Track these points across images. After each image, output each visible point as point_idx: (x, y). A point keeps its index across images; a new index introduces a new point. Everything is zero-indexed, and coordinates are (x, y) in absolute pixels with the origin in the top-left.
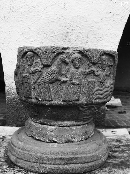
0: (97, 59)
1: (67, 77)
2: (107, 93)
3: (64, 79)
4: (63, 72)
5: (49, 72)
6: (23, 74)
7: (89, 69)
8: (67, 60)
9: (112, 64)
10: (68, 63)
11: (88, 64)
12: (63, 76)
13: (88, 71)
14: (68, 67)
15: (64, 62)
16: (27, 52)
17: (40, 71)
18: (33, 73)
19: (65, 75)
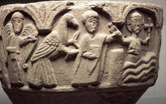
1: (77, 48)
2: (146, 71)
3: (71, 50)
4: (70, 41)
8: (76, 21)
11: (110, 27)
13: (110, 36)
15: (71, 26)
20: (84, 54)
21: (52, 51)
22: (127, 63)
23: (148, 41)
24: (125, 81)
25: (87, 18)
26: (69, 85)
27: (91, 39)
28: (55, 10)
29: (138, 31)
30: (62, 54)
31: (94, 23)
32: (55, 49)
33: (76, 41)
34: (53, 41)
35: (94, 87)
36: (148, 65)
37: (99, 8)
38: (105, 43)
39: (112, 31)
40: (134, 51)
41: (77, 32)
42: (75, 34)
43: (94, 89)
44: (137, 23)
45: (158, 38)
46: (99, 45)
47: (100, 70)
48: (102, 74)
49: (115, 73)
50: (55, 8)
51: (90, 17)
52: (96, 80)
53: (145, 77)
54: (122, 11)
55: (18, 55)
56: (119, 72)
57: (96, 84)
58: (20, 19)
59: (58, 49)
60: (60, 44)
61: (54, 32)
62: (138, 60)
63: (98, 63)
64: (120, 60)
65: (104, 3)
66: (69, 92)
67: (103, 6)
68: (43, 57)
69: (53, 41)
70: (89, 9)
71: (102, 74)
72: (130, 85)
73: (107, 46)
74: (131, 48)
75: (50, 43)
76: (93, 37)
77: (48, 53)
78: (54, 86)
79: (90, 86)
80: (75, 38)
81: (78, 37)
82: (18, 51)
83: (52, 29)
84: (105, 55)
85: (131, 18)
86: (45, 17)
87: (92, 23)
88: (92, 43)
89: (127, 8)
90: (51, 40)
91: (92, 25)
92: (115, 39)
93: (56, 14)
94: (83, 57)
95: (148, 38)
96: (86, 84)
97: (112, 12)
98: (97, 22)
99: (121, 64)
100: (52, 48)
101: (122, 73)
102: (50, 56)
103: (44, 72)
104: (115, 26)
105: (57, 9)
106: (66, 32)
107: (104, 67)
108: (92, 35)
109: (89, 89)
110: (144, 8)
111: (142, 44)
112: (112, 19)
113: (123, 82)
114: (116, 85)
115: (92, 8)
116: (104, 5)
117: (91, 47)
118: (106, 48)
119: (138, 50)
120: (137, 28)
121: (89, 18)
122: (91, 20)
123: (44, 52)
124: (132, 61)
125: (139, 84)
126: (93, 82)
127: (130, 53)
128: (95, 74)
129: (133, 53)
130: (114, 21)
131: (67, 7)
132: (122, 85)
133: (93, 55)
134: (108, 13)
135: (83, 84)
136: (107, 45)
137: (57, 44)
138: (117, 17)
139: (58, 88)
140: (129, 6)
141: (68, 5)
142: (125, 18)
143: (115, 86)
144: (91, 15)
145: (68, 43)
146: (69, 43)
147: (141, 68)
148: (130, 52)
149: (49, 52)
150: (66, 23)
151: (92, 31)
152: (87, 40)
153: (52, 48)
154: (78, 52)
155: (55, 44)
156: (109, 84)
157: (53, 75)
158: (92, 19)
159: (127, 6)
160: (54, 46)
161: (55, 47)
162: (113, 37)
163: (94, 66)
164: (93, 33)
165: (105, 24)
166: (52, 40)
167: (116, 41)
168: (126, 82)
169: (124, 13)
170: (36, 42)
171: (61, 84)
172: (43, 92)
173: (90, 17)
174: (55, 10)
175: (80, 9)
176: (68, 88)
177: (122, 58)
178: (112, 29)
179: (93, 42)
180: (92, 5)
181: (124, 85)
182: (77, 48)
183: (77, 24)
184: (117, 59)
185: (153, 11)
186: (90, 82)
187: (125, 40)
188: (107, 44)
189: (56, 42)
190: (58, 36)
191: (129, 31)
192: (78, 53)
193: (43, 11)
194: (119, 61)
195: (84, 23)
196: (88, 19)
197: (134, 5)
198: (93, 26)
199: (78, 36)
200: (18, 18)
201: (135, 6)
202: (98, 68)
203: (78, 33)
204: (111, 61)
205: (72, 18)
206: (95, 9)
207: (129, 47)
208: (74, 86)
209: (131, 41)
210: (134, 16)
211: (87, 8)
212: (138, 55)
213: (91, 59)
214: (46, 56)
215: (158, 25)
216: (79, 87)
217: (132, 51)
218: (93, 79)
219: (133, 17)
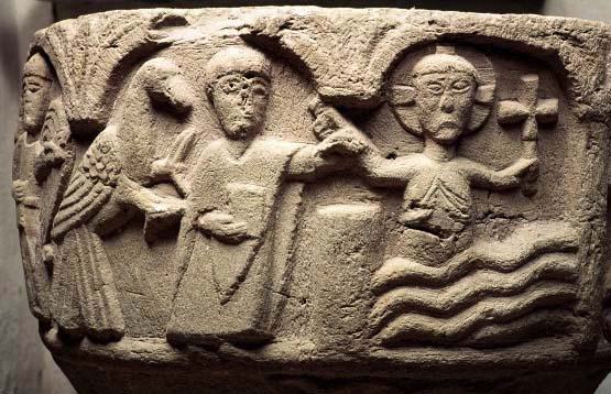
1: (182, 195)
2: (503, 306)
3: (157, 202)
4: (159, 165)
7: (320, 139)
8: (180, 90)
11: (312, 113)
13: (308, 152)
15: (168, 110)
20: (202, 221)
21: (97, 200)
22: (395, 265)
23: (523, 174)
24: (384, 340)
25: (219, 77)
26: (159, 336)
27: (233, 162)
28: (113, 45)
29: (448, 134)
30: (130, 217)
31: (244, 97)
32: (109, 196)
33: (182, 165)
34: (100, 166)
35: (246, 354)
36: (512, 280)
37: (266, 37)
38: (287, 179)
39: (318, 129)
40: (430, 217)
41: (187, 132)
42: (178, 137)
43: (248, 359)
44: (443, 97)
45: (590, 163)
46: (265, 188)
47: (267, 287)
48: (282, 305)
49: (333, 303)
50: (115, 37)
51: (229, 73)
52: (248, 327)
53: (493, 330)
54: (365, 47)
55: (30, 210)
56: (353, 301)
57: (256, 340)
58: (36, 80)
59: (116, 194)
60: (123, 176)
61: (110, 133)
62: (450, 256)
63: (259, 260)
64: (357, 250)
65: (286, 17)
66: (161, 366)
67: (282, 28)
68: (77, 225)
69: (100, 166)
70: (234, 40)
71: (282, 305)
72: (410, 355)
73: (301, 190)
74: (414, 205)
75: (93, 173)
76: (242, 153)
77: (88, 209)
78: (115, 336)
79: (226, 347)
80: (177, 155)
81: (187, 152)
82: (30, 198)
83: (107, 120)
84: (292, 227)
85: (415, 76)
86: (83, 74)
87: (237, 99)
88: (238, 178)
89: (391, 34)
90: (94, 160)
91: (238, 110)
92: (331, 162)
93: (115, 62)
94: (197, 228)
95: (522, 163)
96: (208, 337)
97: (320, 51)
98: (259, 92)
99: (363, 266)
100: (99, 193)
101: (371, 306)
102: (96, 221)
103: (82, 280)
104: (331, 111)
105: (119, 43)
106: (143, 130)
107: (288, 276)
108: (237, 144)
109: (226, 360)
110: (489, 32)
111: (478, 185)
112: (318, 80)
113: (373, 340)
114: (341, 351)
115: (242, 36)
116: (286, 25)
117: (228, 194)
118: (299, 200)
119: (447, 211)
120: (445, 118)
121: (223, 78)
122: (232, 86)
123: (79, 206)
124: (418, 257)
125: (461, 357)
126: (238, 334)
127: (410, 225)
128: (247, 300)
129: (422, 225)
130: (328, 91)
131: (154, 32)
132: (374, 354)
133: (237, 225)
134: (299, 57)
135: (198, 336)
136: (299, 187)
137: (112, 176)
138: (338, 73)
139: (127, 346)
140: (406, 26)
141: (157, 24)
142: (378, 76)
143: (337, 357)
144: (229, 66)
145: (151, 174)
146: (157, 175)
147: (469, 291)
148: (408, 219)
149: (91, 207)
150: (145, 96)
151: (233, 128)
152: (213, 166)
153: (99, 193)
154: (182, 210)
155: (108, 178)
156: (312, 346)
157: (111, 294)
158: (235, 80)
159: (393, 27)
160: (105, 181)
161: (107, 189)
162: (324, 154)
163: (238, 269)
164: (243, 136)
165: (290, 100)
166: (99, 161)
167: (340, 170)
168: (389, 344)
169: (375, 57)
170: (65, 167)
171: (137, 330)
172: (85, 356)
173: (229, 73)
174: (113, 45)
175: (203, 42)
176: (154, 347)
177: (375, 242)
178: (319, 124)
179: (239, 174)
180: (245, 26)
181: (383, 353)
182: (182, 195)
183: (180, 100)
184: (338, 247)
185: (547, 46)
186: (226, 330)
187: (381, 167)
188: (300, 181)
189: (109, 167)
190: (116, 144)
191: (408, 131)
192: (179, 216)
193: (82, 49)
194: (348, 254)
195: (211, 99)
196: (221, 81)
197: (431, 23)
198: (238, 108)
199: (190, 146)
200: (31, 75)
201: (434, 27)
202: (254, 279)
203: (191, 134)
204: (314, 251)
205: (165, 78)
206: (254, 40)
207: (406, 197)
208: (175, 340)
209: (412, 175)
210: (427, 70)
211: (225, 37)
212: (448, 233)
213: (231, 241)
214: (87, 220)
215: (584, 107)
216: (190, 347)
217: (416, 217)
218: (238, 318)
219: (422, 71)
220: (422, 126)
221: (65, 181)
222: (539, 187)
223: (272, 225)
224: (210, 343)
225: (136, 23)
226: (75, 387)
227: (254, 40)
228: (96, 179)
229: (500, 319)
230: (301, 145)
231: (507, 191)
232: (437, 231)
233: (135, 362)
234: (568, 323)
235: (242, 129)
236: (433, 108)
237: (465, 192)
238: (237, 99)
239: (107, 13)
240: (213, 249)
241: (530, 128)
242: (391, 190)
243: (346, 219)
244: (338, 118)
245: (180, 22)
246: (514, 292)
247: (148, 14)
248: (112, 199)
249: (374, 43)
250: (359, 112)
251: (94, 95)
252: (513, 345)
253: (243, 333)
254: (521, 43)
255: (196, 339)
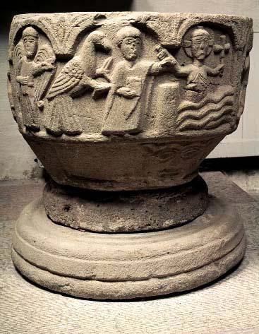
0: (179, 37)
1: (109, 81)
2: (215, 115)
3: (100, 85)
4: (99, 71)
5: (67, 70)
6: (97, 70)
7: (161, 60)
8: (106, 43)
9: (228, 45)
10: (251, 20)
11: (157, 51)
12: (100, 79)
13: (157, 65)
14: (109, 59)
15: (100, 50)
16: (24, 27)
17: (50, 70)
18: (37, 74)
19: (102, 76)
20: (118, 91)
30: (87, 90)
31: (134, 45)
32: (78, 83)
34: (74, 71)
36: (218, 106)
39: (160, 56)
43: (134, 138)
46: (140, 78)
53: (214, 123)
59: (81, 82)
61: (77, 58)
63: (140, 104)
69: (74, 71)
72: (188, 133)
74: (191, 82)
78: (78, 133)
79: (127, 135)
81: (110, 66)
87: (131, 46)
89: (186, 22)
91: (131, 49)
93: (79, 32)
94: (116, 94)
95: (220, 66)
98: (138, 44)
101: (177, 118)
102: (71, 92)
108: (130, 63)
111: (209, 74)
116: (149, 19)
120: (202, 52)
123: (63, 86)
124: (192, 100)
127: (190, 89)
128: (135, 118)
129: (193, 89)
130: (164, 43)
135: (116, 132)
136: (153, 78)
137: (80, 75)
139: (84, 137)
141: (96, 18)
146: (98, 75)
160: (76, 77)
162: (163, 66)
163: (132, 108)
164: (132, 60)
165: (150, 47)
167: (168, 71)
168: (182, 130)
169: (180, 30)
176: (97, 136)
177: (176, 96)
181: (180, 133)
182: (109, 81)
184: (167, 98)
187: (182, 70)
189: (78, 72)
191: (188, 56)
192: (109, 88)
196: (125, 40)
202: (138, 109)
206: (136, 24)
209: (190, 72)
213: (129, 98)
218: (132, 125)
220: (193, 54)
221: (52, 78)
222: (224, 74)
223: (144, 91)
224: (120, 135)
225: (88, 17)
226: (31, 146)
227: (136, 24)
228: (72, 76)
229: (215, 119)
230: (153, 62)
231: (215, 76)
232: (198, 91)
233: (87, 142)
234: (230, 119)
235: (133, 57)
236: (198, 48)
237: (205, 76)
238: (131, 46)
239: (71, 13)
240: (122, 101)
241: (223, 53)
242: (184, 77)
243: (170, 88)
244: (168, 53)
245: (103, 17)
246: (219, 110)
247: (94, 14)
248: (80, 83)
249: (179, 26)
250: (173, 50)
251: (69, 45)
252: (217, 127)
253: (134, 130)
254: (222, 25)
255: (115, 133)
